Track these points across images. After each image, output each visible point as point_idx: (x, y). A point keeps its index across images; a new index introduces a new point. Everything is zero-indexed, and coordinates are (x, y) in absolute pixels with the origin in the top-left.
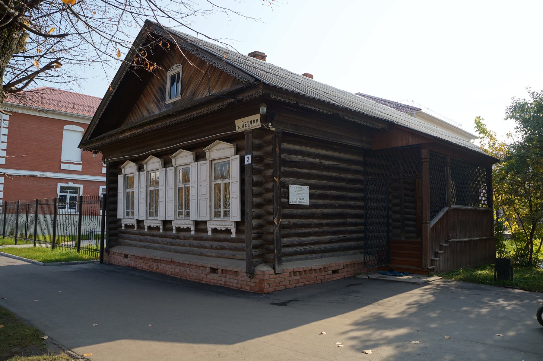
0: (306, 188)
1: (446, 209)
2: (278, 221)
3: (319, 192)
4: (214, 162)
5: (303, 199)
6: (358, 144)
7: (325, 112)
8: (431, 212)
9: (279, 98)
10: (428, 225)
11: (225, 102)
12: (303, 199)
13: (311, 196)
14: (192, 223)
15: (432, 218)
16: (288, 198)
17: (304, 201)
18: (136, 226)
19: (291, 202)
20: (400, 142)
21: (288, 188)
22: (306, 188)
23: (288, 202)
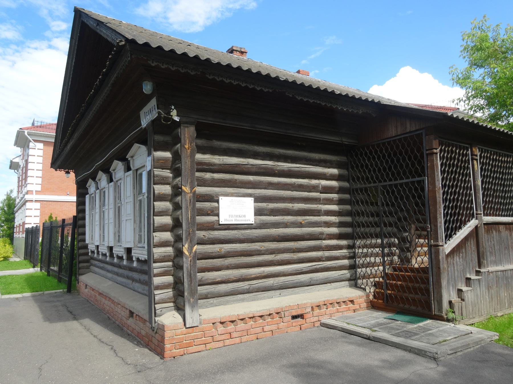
0: (251, 200)
1: (472, 223)
2: (190, 249)
3: (264, 205)
4: (139, 172)
5: (245, 216)
6: (338, 139)
7: (259, 89)
8: (446, 229)
9: (330, 105)
10: (441, 248)
11: (109, 85)
12: (245, 216)
13: (258, 212)
14: (123, 250)
15: (449, 237)
16: (218, 215)
17: (247, 218)
18: (108, 255)
19: (223, 221)
20: (393, 131)
21: (218, 201)
22: (251, 200)
23: (219, 221)
